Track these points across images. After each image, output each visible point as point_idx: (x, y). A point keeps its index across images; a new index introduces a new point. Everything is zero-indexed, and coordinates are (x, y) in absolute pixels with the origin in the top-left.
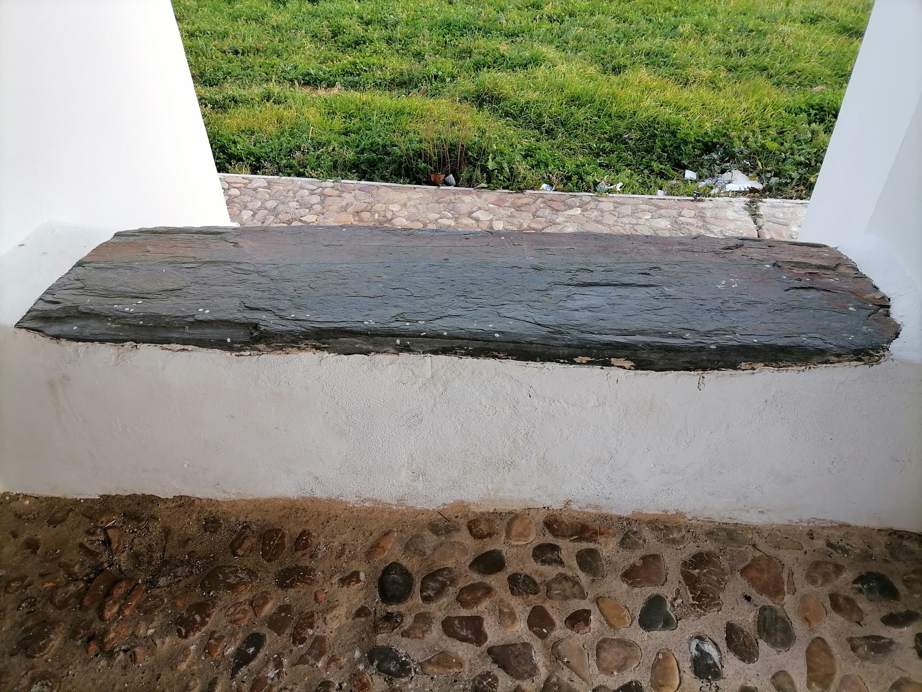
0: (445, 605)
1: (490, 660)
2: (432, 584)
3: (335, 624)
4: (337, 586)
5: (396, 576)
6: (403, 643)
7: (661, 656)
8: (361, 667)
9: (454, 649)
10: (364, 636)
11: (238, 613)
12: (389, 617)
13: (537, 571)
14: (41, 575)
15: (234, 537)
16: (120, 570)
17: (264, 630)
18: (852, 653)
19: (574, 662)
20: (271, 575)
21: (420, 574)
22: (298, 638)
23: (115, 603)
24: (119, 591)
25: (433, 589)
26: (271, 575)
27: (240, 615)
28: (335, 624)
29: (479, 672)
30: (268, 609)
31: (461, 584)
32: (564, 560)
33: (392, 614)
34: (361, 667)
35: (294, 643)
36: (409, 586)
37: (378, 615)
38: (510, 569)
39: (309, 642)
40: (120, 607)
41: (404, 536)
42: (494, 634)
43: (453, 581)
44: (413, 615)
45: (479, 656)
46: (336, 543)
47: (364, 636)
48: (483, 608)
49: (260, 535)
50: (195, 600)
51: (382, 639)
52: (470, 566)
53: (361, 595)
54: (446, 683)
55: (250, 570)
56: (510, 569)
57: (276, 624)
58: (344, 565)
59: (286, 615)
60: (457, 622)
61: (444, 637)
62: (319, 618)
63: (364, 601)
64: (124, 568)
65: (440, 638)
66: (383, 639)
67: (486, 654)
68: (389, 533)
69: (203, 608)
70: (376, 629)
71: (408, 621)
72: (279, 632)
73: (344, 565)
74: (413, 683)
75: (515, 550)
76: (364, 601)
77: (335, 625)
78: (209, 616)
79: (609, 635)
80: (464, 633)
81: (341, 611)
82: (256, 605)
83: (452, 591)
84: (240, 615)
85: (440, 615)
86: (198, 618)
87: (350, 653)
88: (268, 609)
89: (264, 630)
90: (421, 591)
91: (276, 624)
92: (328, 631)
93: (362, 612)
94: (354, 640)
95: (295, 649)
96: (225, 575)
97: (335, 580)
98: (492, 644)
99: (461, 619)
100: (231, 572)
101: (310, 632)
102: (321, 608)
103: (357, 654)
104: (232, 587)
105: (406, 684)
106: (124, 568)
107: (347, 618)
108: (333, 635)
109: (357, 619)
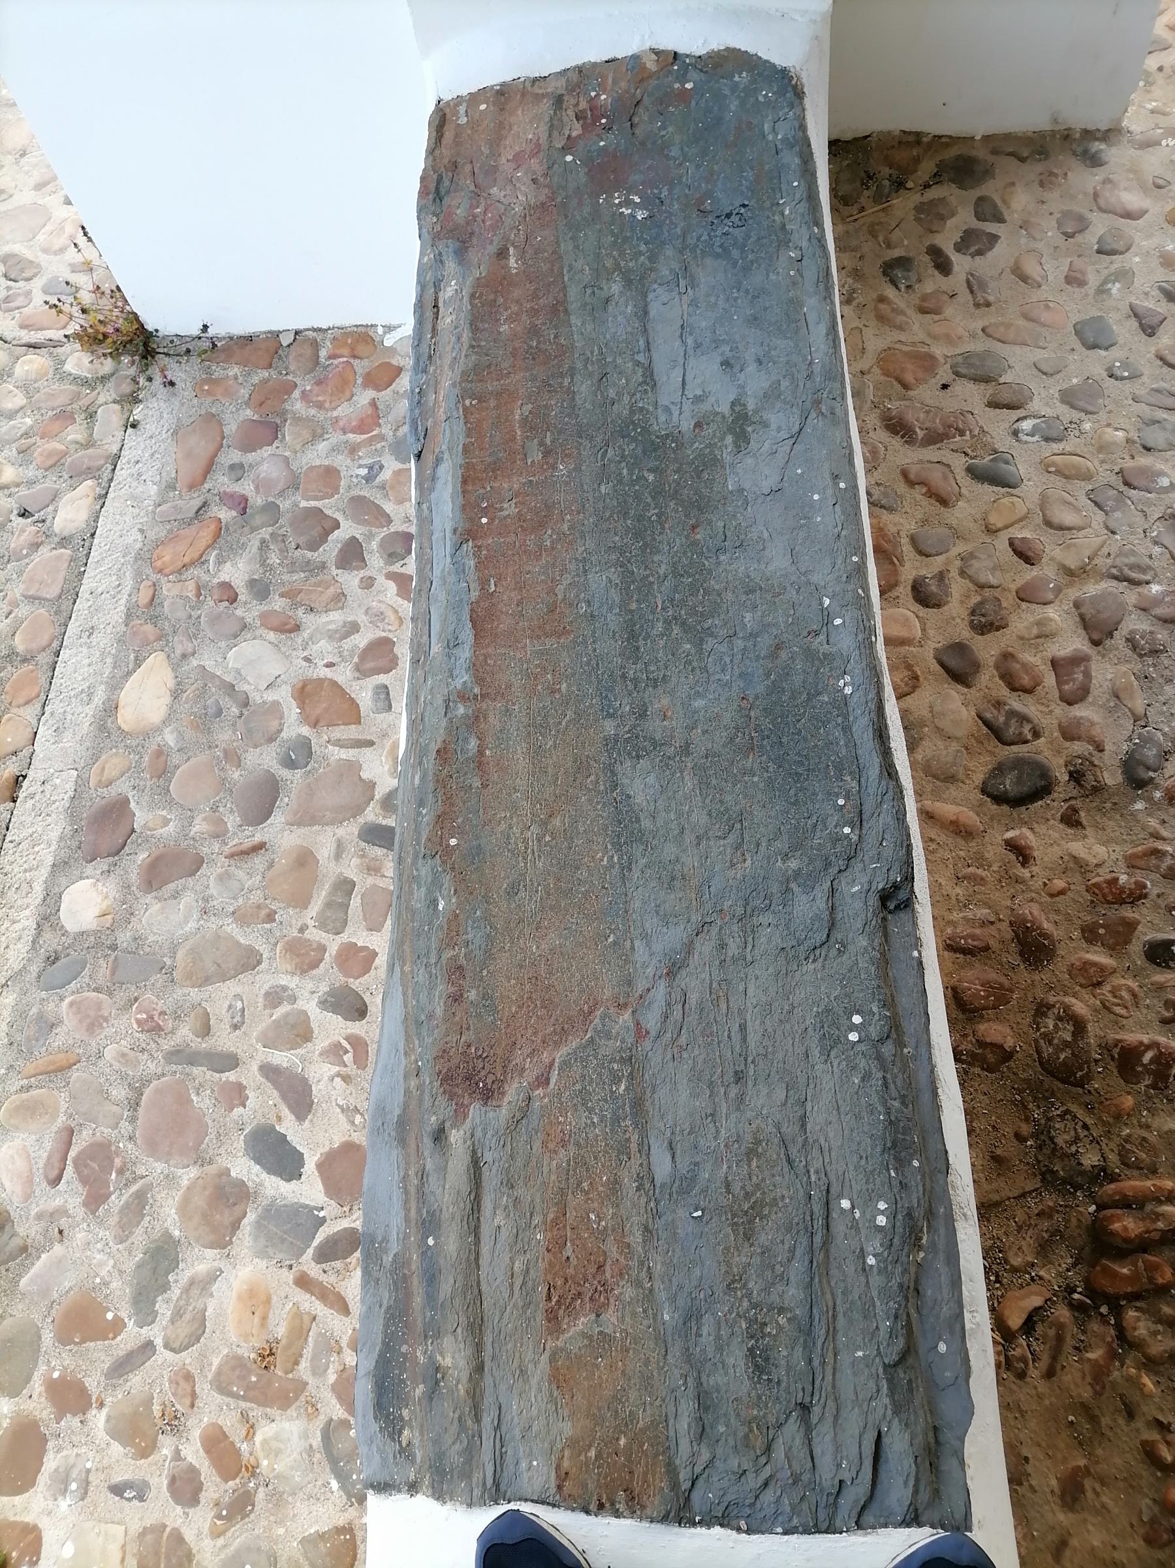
0: (1041, 708)
1: (1108, 642)
2: (1012, 730)
3: (1101, 850)
4: (1034, 868)
5: (1008, 782)
6: (1114, 748)
7: (1052, 469)
8: (1158, 795)
9: (858, 904)
10: (1108, 805)
11: (1121, 998)
12: (1076, 777)
13: (962, 602)
14: (1131, 1415)
15: (977, 1070)
16: (1074, 1265)
17: (1136, 948)
18: (993, 308)
19: (1088, 553)
20: (1037, 978)
21: (997, 750)
22: (1137, 896)
23: (1158, 1216)
24: (1127, 1225)
25: (1021, 726)
26: (1037, 978)
27: (1124, 994)
28: (1101, 850)
29: (1129, 652)
30: (1098, 956)
31: (1003, 692)
32: (936, 571)
33: (1071, 774)
34: (1158, 795)
35: (1145, 896)
36: (1019, 764)
37: (1075, 793)
38: (963, 633)
39: (1139, 876)
40: (1160, 1202)
41: (929, 787)
42: (1072, 643)
43: (998, 704)
44: (1068, 744)
45: (1103, 656)
46: (958, 890)
47: (1108, 805)
48: (1034, 659)
49: (969, 1020)
50: (1116, 1080)
51: (1112, 777)
52: (968, 686)
53: (1041, 829)
54: (1150, 688)
55: (1035, 1016)
56: (963, 633)
57: (1118, 936)
58: (995, 868)
59: (1102, 926)
60: (1066, 687)
61: (1090, 699)
62: (1098, 875)
63: (1052, 822)
64: (1069, 1261)
65: (1093, 704)
66: (1113, 775)
67: (1100, 648)
68: (927, 813)
69: (1127, 1060)
70: (1098, 789)
71: (1078, 747)
72: (1131, 926)
73: (995, 868)
74: (1161, 726)
75: (931, 633)
76: (1052, 822)
77: (1101, 851)
78: (1141, 1043)
79: (1039, 520)
80: (1080, 677)
81: (1077, 848)
82: (1092, 978)
83: (1016, 703)
84: (1124, 994)
85: (1060, 711)
86: (1148, 1057)
87: (1140, 816)
88: (1098, 956)
89: (1136, 948)
90: (1026, 742)
91: (1118, 936)
92: (1113, 856)
93: (1071, 820)
94: (1118, 817)
95: (1155, 891)
96: (1058, 1050)
97: (1025, 873)
98: (1086, 642)
99: (1059, 683)
100: (1050, 1042)
101: (1123, 878)
102: (1077, 878)
103: (1139, 806)
104: (1080, 1027)
105: (1164, 734)
106: (1069, 1261)
107: (1085, 837)
108: (1118, 848)
109: (1084, 822)
